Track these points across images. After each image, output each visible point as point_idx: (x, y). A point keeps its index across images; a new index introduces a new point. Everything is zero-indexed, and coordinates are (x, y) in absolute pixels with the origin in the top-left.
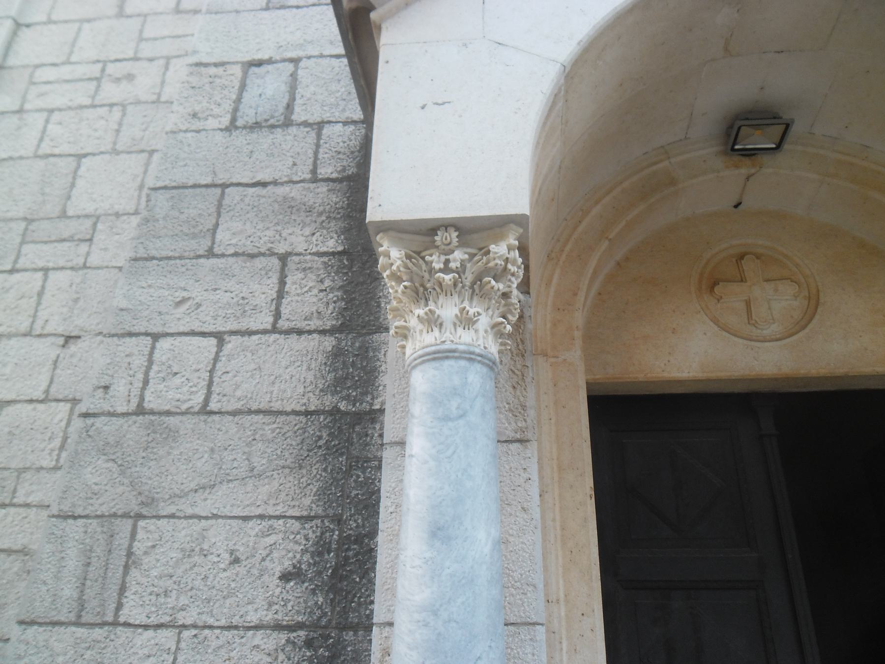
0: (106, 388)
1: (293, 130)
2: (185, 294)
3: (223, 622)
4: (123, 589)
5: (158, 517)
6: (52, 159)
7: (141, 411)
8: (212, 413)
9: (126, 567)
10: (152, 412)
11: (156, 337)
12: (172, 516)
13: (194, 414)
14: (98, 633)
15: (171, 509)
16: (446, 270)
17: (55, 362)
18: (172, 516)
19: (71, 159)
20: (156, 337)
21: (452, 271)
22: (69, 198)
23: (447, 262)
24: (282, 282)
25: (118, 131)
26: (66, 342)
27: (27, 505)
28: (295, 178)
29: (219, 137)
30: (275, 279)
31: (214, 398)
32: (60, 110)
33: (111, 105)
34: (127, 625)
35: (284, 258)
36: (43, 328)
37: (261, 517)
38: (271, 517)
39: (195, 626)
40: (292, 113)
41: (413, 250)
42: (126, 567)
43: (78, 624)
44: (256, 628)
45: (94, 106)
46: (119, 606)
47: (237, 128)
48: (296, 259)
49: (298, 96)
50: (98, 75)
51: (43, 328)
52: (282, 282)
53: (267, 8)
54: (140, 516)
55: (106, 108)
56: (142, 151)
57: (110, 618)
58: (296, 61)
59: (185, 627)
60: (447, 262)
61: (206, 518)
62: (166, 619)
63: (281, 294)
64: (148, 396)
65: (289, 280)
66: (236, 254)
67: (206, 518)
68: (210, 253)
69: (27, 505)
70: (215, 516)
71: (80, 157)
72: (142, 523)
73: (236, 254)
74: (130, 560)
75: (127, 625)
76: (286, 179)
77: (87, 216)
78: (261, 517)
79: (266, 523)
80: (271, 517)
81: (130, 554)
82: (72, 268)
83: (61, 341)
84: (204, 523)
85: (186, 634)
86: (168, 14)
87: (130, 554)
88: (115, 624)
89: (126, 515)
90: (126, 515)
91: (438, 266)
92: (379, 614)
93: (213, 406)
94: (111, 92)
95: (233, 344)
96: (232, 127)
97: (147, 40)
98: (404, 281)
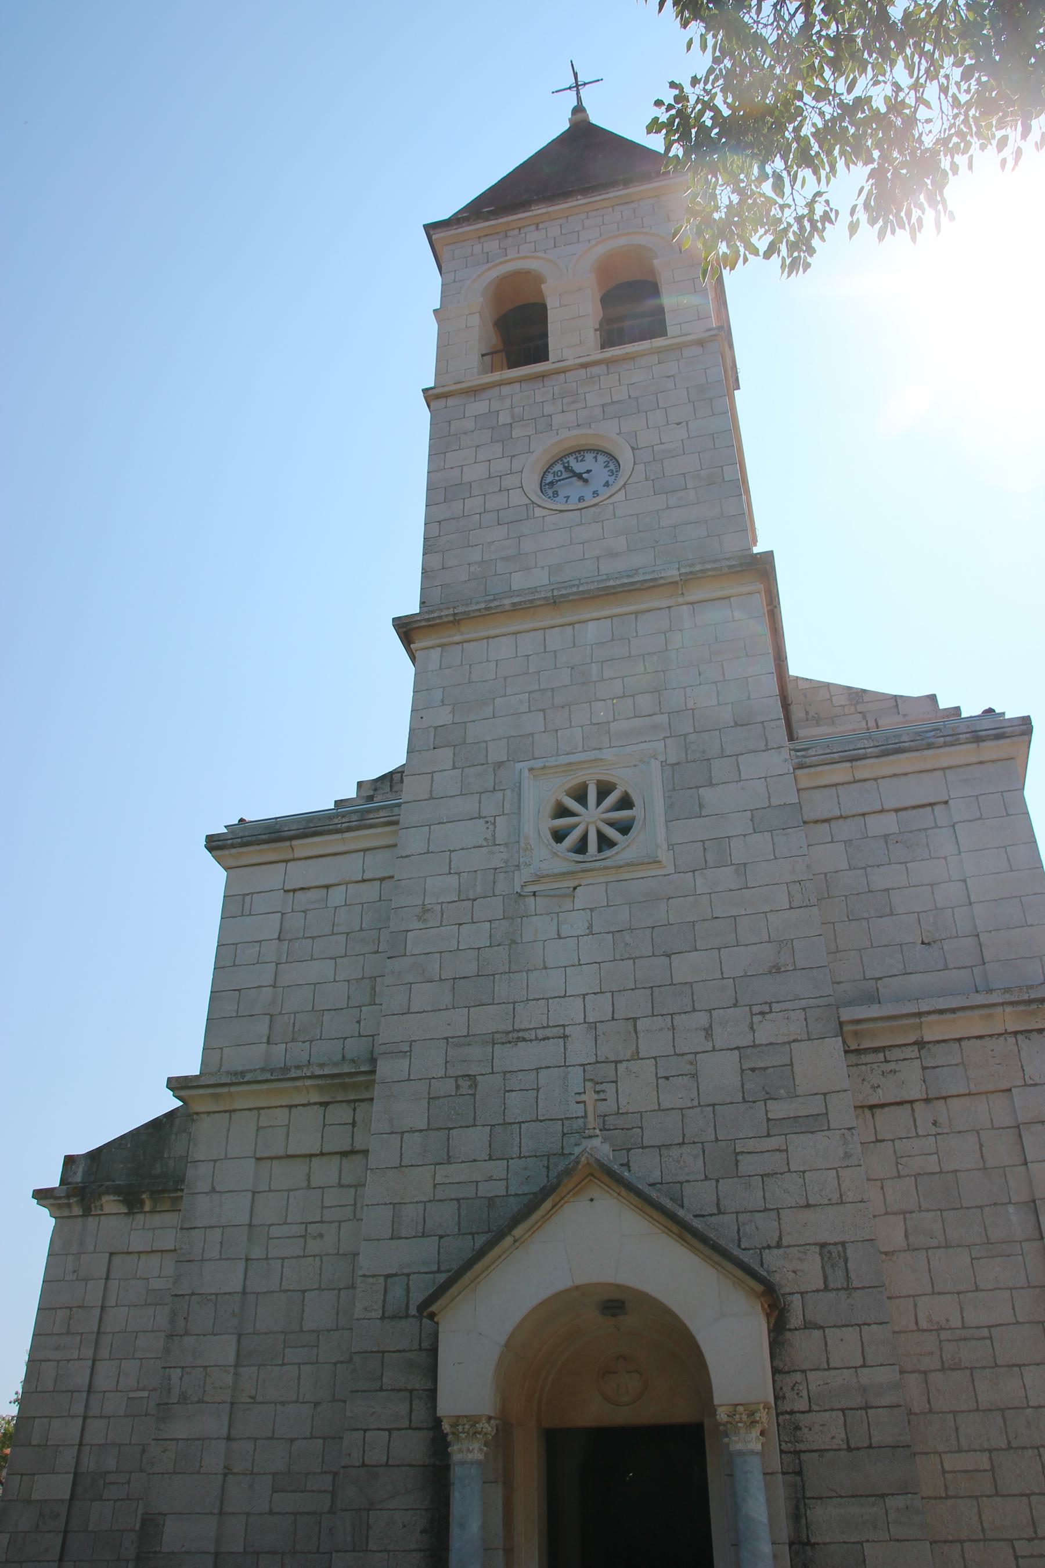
0: (349, 1455)
1: (410, 1319)
2: (374, 1410)
3: (402, 1549)
4: (367, 1538)
5: (377, 1510)
6: (289, 1293)
7: (364, 1465)
8: (390, 1466)
9: (368, 1530)
10: (368, 1466)
11: (365, 1431)
12: (381, 1509)
13: (383, 1466)
14: (361, 1554)
15: (379, 1507)
16: (463, 1432)
17: (312, 1417)
18: (381, 1509)
19: (299, 1293)
20: (365, 1431)
21: (464, 1433)
22: (302, 1319)
23: (464, 1428)
24: (411, 1405)
25: (320, 1274)
26: (315, 1405)
27: (313, 1491)
28: (413, 1349)
29: (378, 1322)
30: (408, 1403)
31: (390, 1459)
32: (288, 1258)
33: (314, 1256)
34: (370, 1551)
35: (411, 1391)
36: (304, 1398)
37: (412, 1509)
38: (415, 1509)
39: (393, 1551)
40: (408, 1309)
41: (847, 170)
42: (368, 1530)
43: (354, 1551)
44: (413, 1551)
45: (304, 1256)
46: (367, 1545)
47: (386, 1318)
48: (416, 1392)
49: (410, 1298)
50: (304, 1234)
51: (304, 1398)
52: (411, 1405)
53: (392, 1239)
54: (369, 1510)
55: (312, 1258)
56: (334, 1289)
57: (365, 1548)
58: (408, 1275)
59: (390, 1551)
60: (464, 1428)
61: (393, 1510)
62: (383, 1548)
63: (411, 1410)
64: (366, 1459)
65: (414, 1403)
66: (391, 1390)
67: (393, 1510)
68: (381, 1389)
69: (313, 1491)
70: (396, 1509)
71: (304, 1292)
72: (370, 1512)
73: (391, 1390)
74: (369, 1527)
75: (370, 1551)
76: (409, 1349)
77: (313, 1331)
78: (412, 1509)
79: (413, 1512)
80: (415, 1509)
81: (368, 1524)
82: (311, 1363)
83: (313, 1405)
84: (392, 1512)
85: (391, 1553)
86: (336, 1187)
87: (368, 1524)
88: (367, 1551)
89: (365, 1509)
90: (365, 1509)
91: (460, 1430)
92: (450, 1548)
93: (390, 1463)
94: (314, 1247)
95: (395, 1433)
96: (383, 1318)
97: (327, 1207)
98: (914, 7)
